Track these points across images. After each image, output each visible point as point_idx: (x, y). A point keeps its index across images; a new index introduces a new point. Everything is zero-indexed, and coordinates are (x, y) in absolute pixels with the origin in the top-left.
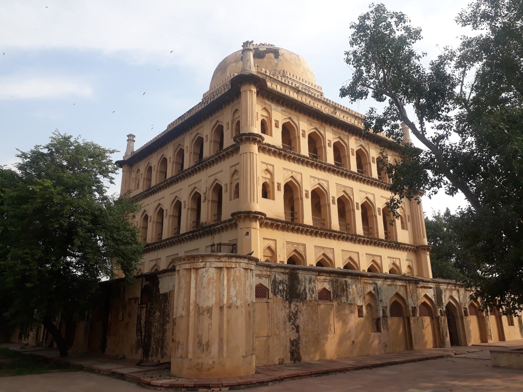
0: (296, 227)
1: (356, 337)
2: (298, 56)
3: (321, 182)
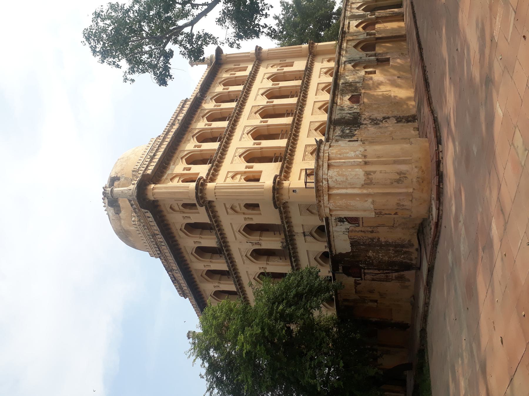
0: (289, 151)
1: (394, 75)
2: (118, 160)
3: (246, 131)
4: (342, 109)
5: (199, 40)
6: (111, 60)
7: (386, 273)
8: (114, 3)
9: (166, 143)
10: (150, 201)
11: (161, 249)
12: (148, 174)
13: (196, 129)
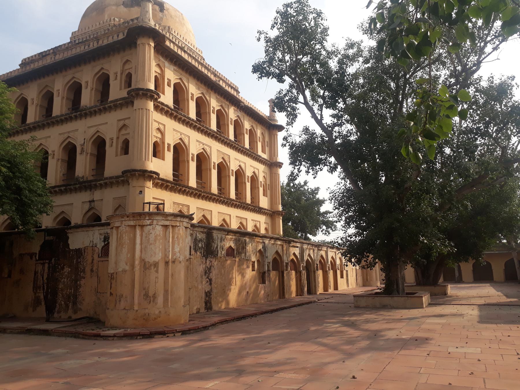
1: (250, 288)
2: (182, 14)
3: (206, 147)
4: (222, 240)
5: (291, 109)
6: (279, 21)
7: (44, 286)
8: (329, 32)
9: (196, 65)
10: (136, 39)
11: (80, 45)
12: (165, 42)
13: (210, 97)
